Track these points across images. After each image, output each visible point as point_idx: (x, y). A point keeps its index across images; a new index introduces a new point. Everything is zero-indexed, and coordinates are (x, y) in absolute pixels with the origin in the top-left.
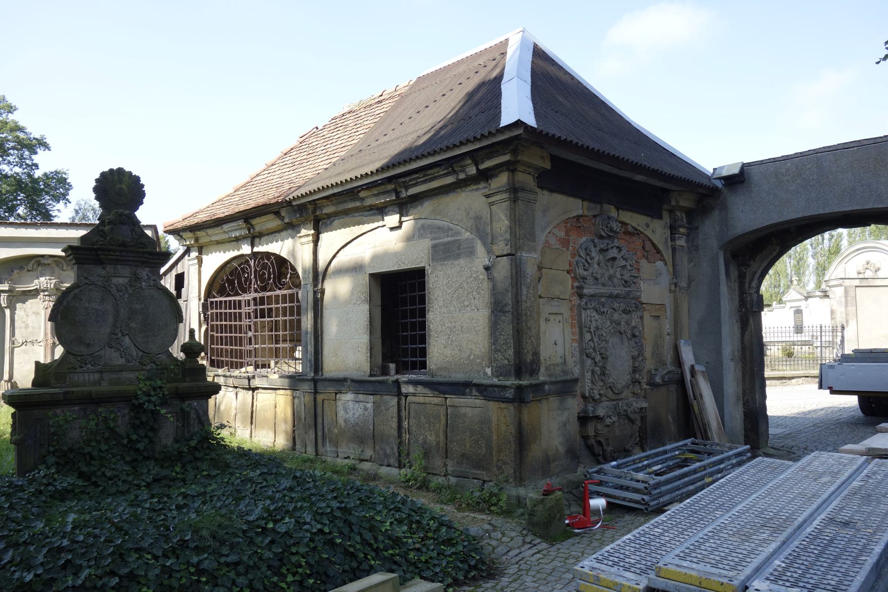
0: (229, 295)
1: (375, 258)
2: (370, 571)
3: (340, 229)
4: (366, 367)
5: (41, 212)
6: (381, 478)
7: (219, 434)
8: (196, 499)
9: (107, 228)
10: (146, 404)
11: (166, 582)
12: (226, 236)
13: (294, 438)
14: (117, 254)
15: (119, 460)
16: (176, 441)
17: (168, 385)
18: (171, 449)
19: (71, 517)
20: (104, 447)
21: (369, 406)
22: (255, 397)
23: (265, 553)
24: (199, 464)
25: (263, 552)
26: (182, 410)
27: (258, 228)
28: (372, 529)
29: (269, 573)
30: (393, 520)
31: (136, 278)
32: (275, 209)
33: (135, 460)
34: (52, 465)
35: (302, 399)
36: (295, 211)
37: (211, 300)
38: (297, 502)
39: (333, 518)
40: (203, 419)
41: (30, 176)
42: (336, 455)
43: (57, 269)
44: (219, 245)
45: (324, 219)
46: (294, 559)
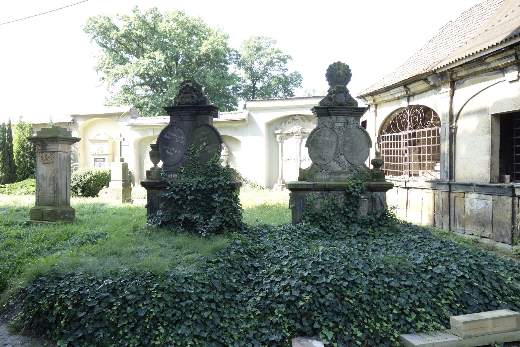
0: (393, 132)
1: (496, 104)
2: (498, 307)
3: (470, 85)
4: (488, 177)
5: (289, 94)
6: (497, 250)
7: (392, 212)
8: (382, 247)
9: (332, 96)
10: (353, 193)
11: (371, 289)
12: (392, 97)
13: (434, 219)
14: (338, 110)
15: (339, 222)
16: (369, 214)
17: (364, 183)
18: (366, 218)
19: (321, 248)
20: (332, 214)
21: (490, 202)
22: (409, 193)
23: (428, 283)
24: (382, 228)
25: (426, 283)
26: (372, 197)
27: (412, 91)
28: (498, 281)
29: (430, 295)
30: (513, 277)
31: (348, 123)
32: (424, 77)
33: (348, 222)
34: (308, 221)
35: (441, 196)
36: (438, 77)
37: (383, 135)
38: (445, 257)
39: (471, 271)
40: (383, 203)
41: (284, 75)
42: (463, 232)
43: (301, 122)
44: (388, 103)
45: (458, 80)
46: (446, 290)
